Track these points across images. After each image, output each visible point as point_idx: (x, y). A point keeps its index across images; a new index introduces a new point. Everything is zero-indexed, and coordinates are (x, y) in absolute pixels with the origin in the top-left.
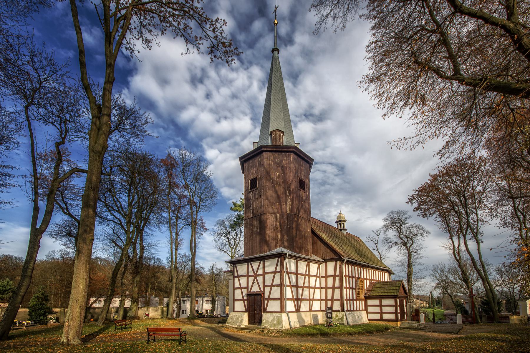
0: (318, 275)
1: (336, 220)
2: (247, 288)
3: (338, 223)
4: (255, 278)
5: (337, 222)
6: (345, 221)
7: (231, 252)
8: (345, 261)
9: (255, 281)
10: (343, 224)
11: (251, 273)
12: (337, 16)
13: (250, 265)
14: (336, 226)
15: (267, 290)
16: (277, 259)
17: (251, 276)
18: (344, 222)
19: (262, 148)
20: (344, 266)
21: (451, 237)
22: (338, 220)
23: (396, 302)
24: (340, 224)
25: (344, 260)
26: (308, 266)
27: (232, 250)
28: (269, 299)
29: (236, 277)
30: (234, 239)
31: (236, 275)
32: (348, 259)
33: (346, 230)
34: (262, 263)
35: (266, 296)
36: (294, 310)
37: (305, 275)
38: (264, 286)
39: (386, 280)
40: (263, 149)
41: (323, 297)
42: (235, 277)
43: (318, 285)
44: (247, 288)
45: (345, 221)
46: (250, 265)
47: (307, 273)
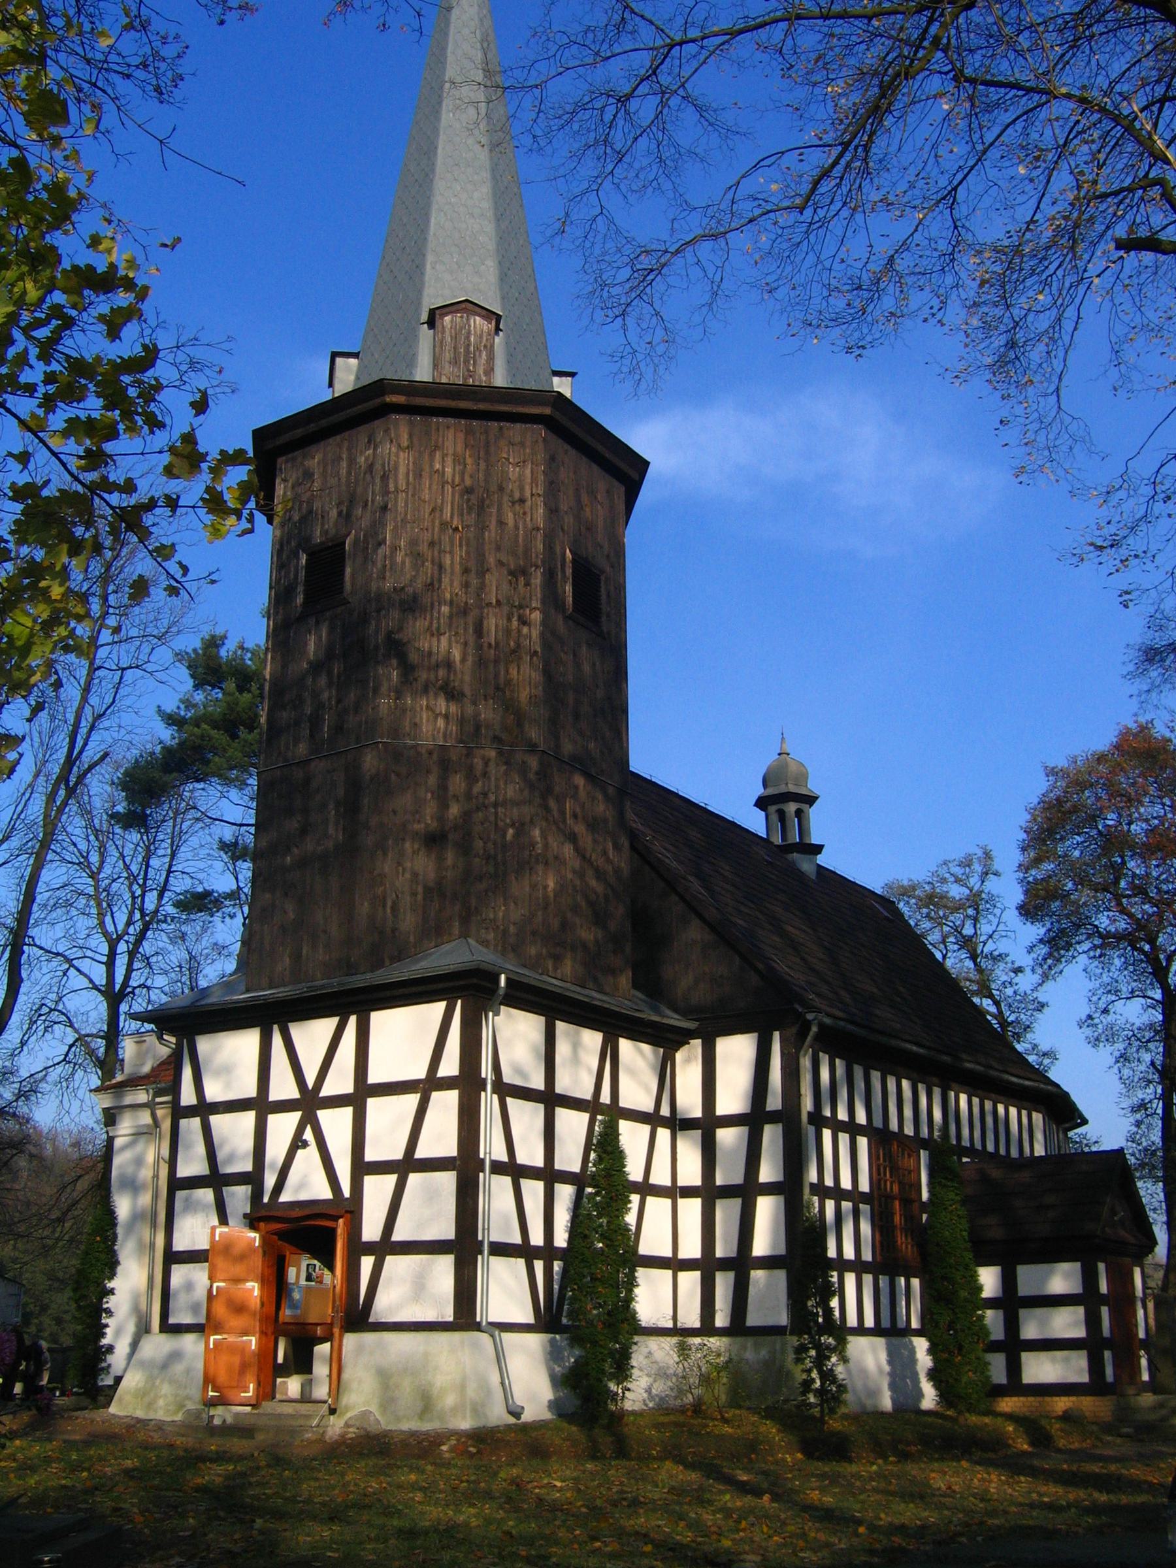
0: (665, 1111)
1: (759, 791)
2: (254, 1179)
3: (772, 809)
4: (310, 1120)
5: (762, 803)
6: (811, 800)
7: (110, 964)
8: (814, 1029)
9: (308, 1135)
10: (799, 813)
11: (283, 1087)
12: (957, 1310)
13: (277, 1041)
14: (755, 822)
15: (378, 1190)
16: (441, 1006)
17: (284, 1106)
18: (804, 807)
19: (383, 394)
20: (806, 1062)
21: (394, 930)
22: (771, 791)
23: (1089, 1278)
24: (782, 815)
25: (805, 1027)
26: (610, 1053)
27: (112, 955)
28: (386, 1247)
29: (191, 1112)
30: (132, 879)
31: (188, 1097)
32: (827, 1021)
33: (818, 849)
34: (353, 1020)
35: (371, 1231)
36: (527, 1317)
37: (590, 1106)
38: (361, 1168)
39: (1039, 1151)
40: (389, 399)
41: (691, 1248)
42: (179, 1112)
43: (660, 1177)
44: (254, 1179)
45: (811, 800)
46: (277, 1041)
47: (605, 1098)
